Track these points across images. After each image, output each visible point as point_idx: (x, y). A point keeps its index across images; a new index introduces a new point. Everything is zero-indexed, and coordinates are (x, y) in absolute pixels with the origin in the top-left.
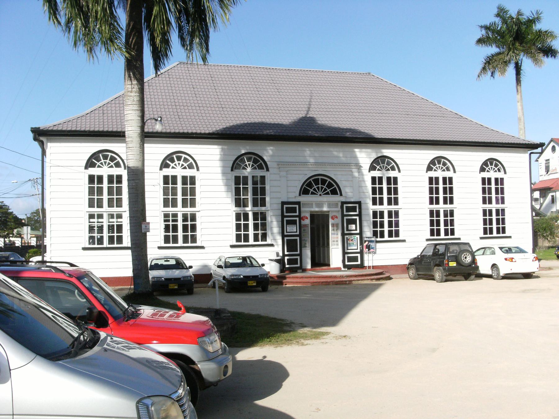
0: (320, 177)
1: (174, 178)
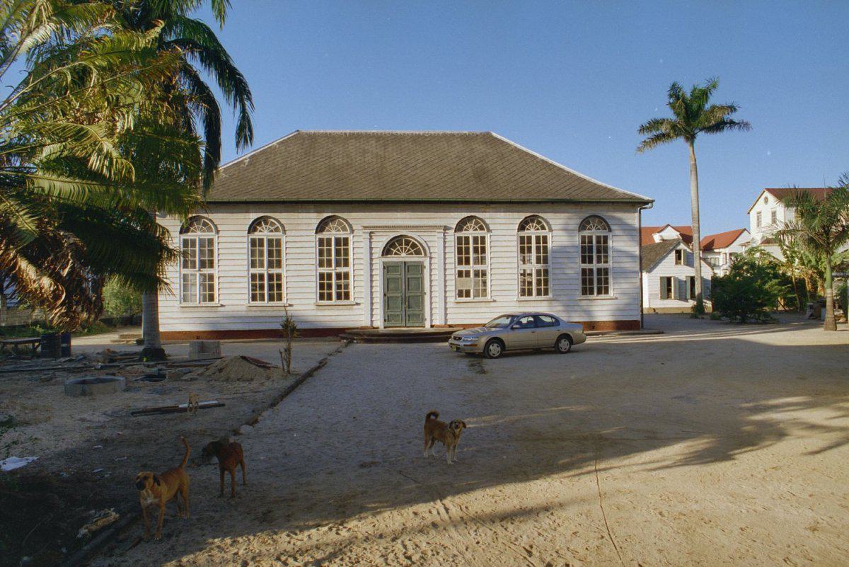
1: (261, 241)
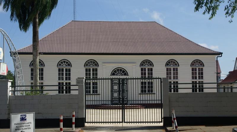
0: (119, 69)
